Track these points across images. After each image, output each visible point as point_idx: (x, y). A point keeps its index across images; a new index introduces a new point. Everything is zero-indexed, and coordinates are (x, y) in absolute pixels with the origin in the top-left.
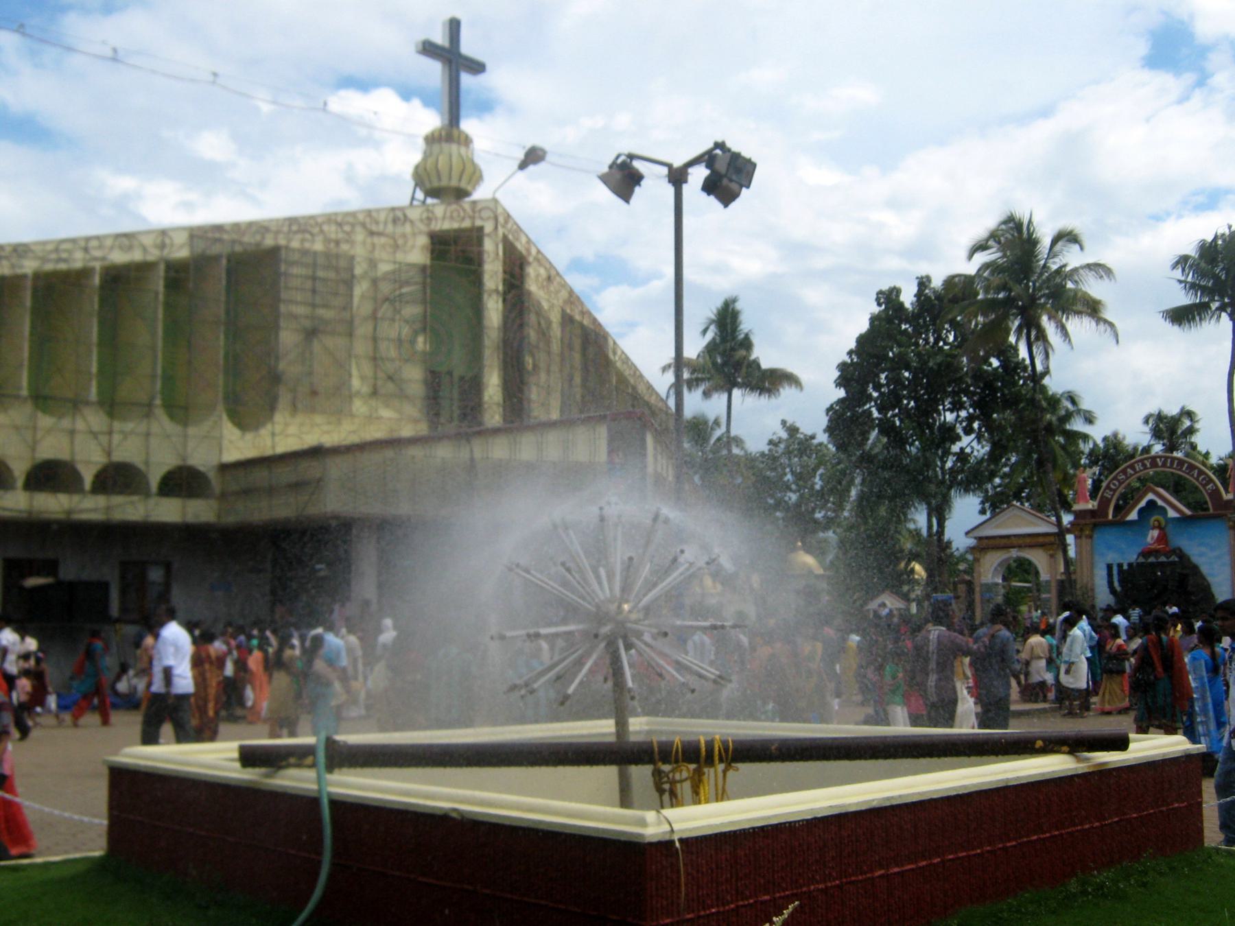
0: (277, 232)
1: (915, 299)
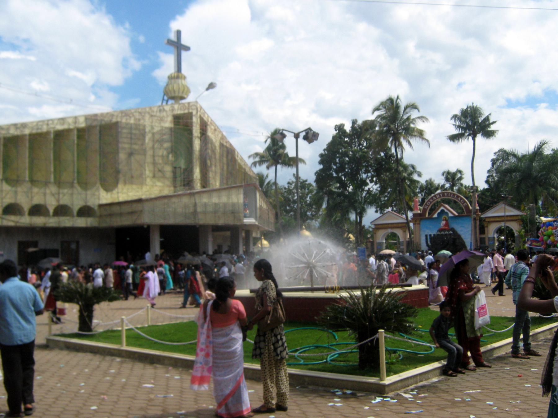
0: (117, 116)
1: (351, 129)
